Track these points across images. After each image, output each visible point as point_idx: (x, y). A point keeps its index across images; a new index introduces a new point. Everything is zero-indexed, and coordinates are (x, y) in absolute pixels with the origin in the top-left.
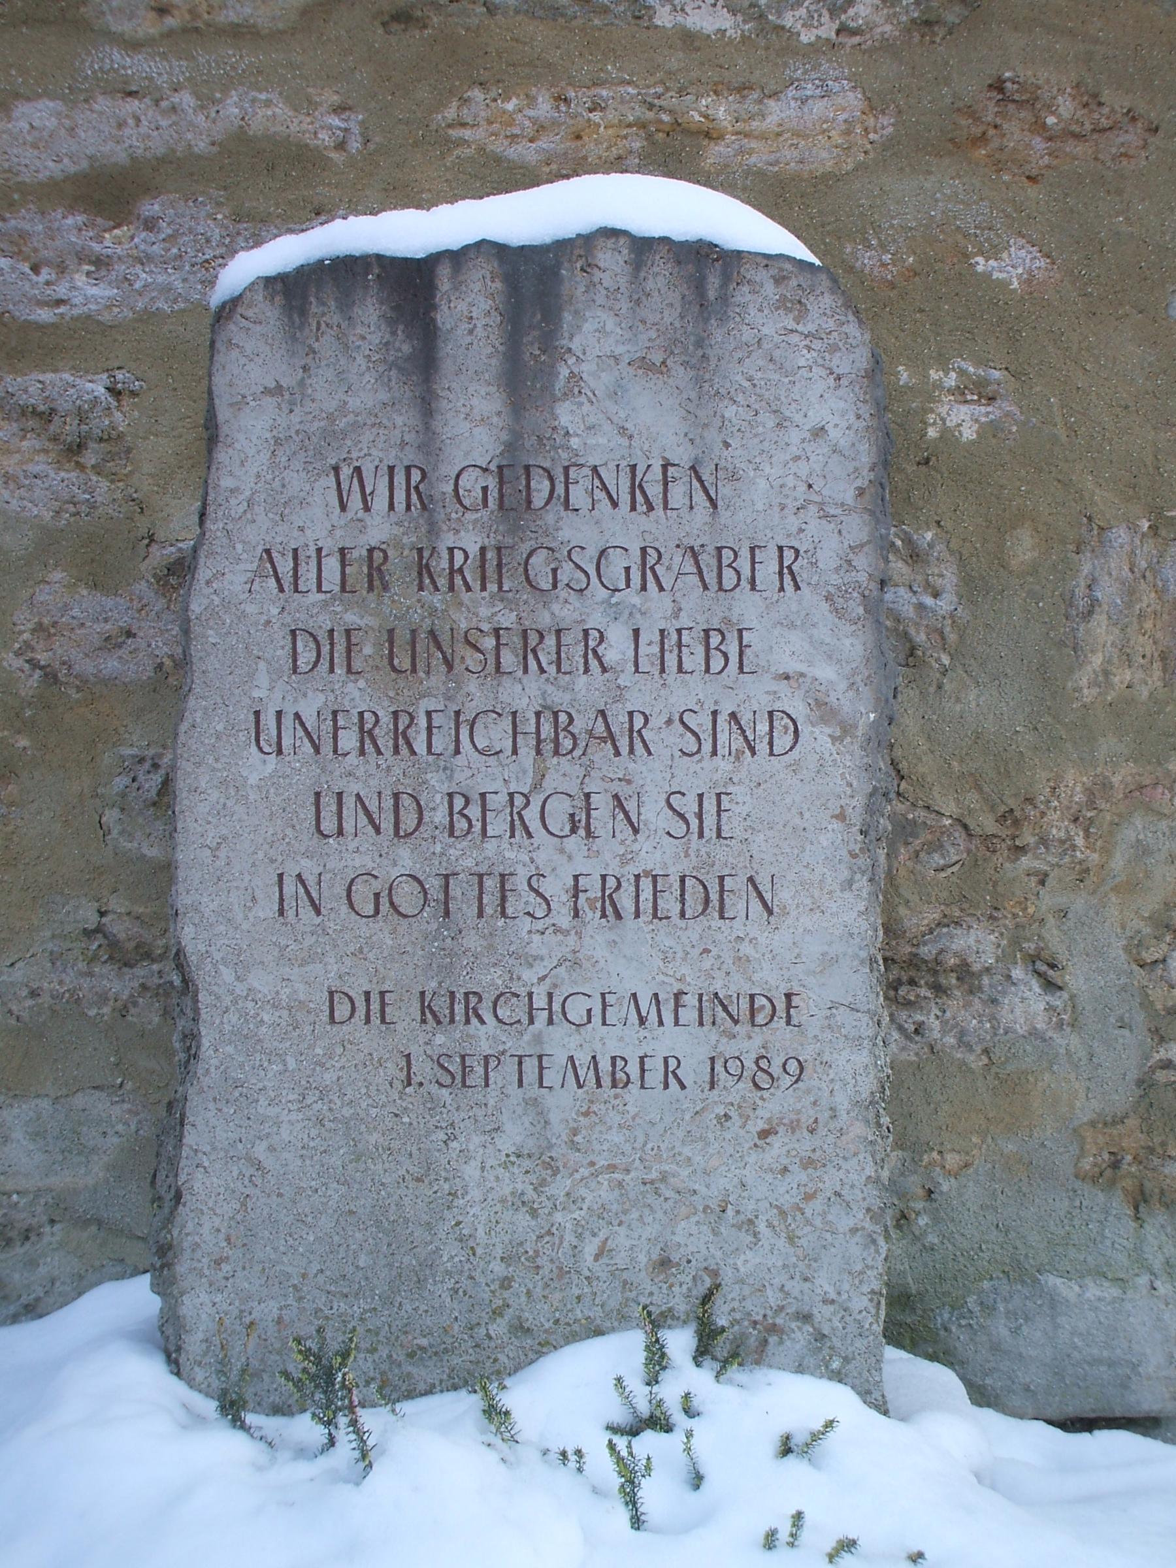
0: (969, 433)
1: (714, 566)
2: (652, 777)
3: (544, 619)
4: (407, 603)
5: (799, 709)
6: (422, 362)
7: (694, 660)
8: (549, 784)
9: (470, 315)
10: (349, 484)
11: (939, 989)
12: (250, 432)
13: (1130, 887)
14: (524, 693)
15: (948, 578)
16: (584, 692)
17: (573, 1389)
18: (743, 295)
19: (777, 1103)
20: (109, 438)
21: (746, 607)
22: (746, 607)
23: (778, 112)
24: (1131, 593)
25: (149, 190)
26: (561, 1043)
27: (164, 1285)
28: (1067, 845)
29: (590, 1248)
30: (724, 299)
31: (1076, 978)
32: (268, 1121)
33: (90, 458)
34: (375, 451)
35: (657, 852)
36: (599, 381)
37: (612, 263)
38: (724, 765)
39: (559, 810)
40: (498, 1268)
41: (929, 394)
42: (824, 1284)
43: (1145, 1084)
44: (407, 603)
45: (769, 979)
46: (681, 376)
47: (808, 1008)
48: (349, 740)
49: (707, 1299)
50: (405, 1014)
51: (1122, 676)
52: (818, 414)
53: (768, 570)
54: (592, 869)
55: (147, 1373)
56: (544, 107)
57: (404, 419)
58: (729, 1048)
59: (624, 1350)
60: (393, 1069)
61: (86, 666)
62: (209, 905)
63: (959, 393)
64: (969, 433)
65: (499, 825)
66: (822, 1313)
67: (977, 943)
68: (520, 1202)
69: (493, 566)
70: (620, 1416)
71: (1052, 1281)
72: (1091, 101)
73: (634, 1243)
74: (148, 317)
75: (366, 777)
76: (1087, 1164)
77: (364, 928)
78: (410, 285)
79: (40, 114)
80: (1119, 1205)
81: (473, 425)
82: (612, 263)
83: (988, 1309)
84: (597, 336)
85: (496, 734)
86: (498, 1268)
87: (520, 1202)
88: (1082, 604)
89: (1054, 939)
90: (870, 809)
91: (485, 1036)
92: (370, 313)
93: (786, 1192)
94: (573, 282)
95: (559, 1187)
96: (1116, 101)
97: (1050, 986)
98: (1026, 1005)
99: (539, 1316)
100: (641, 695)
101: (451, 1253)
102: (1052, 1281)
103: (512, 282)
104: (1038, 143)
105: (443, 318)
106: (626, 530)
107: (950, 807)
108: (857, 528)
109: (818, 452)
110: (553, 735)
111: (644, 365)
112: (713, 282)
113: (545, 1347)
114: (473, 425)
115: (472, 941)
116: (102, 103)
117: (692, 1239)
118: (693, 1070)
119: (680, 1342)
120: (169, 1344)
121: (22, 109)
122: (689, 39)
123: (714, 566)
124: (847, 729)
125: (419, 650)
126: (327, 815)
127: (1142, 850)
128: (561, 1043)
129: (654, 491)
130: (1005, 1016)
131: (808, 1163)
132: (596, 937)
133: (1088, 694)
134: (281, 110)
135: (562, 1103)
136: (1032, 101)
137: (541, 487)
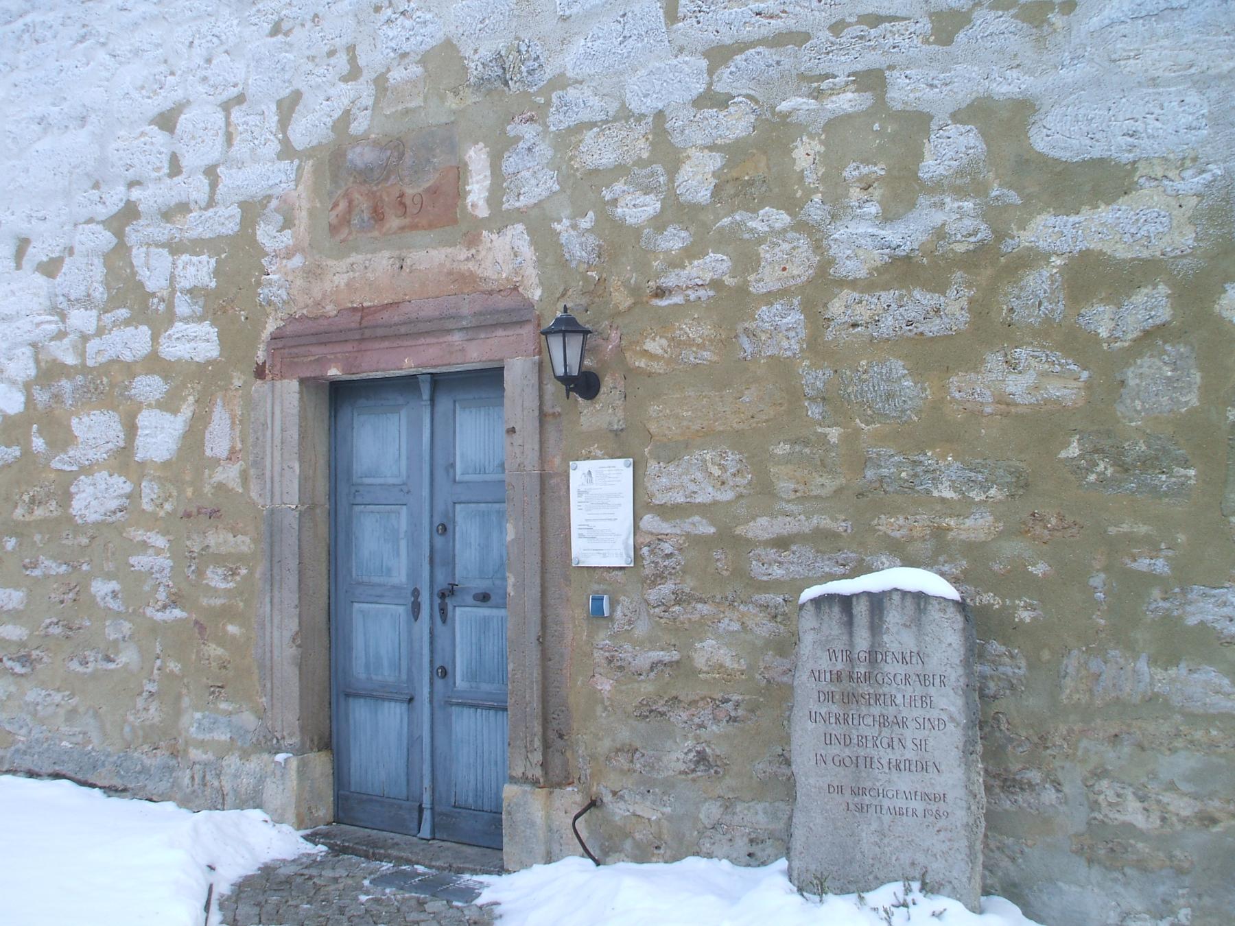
0: (1028, 620)
1: (923, 679)
2: (909, 734)
3: (881, 691)
4: (847, 686)
5: (945, 718)
6: (849, 623)
7: (919, 704)
8: (883, 734)
9: (861, 610)
10: (832, 654)
11: (1022, 789)
12: (808, 640)
13: (1083, 761)
14: (876, 710)
15: (1023, 663)
16: (891, 711)
17: (884, 895)
18: (930, 607)
19: (942, 823)
20: (784, 614)
21: (932, 691)
22: (932, 691)
23: (969, 522)
24: (1078, 671)
25: (794, 543)
26: (886, 803)
27: (788, 859)
28: (1061, 746)
29: (894, 858)
30: (925, 609)
31: (1066, 789)
32: (814, 817)
33: (779, 619)
34: (839, 645)
35: (910, 754)
36: (893, 629)
37: (896, 597)
38: (927, 732)
39: (885, 741)
40: (871, 861)
41: (1015, 608)
42: (955, 874)
43: (1089, 824)
44: (847, 686)
45: (939, 790)
46: (914, 628)
47: (949, 797)
48: (833, 720)
49: (924, 875)
50: (847, 792)
51: (1076, 697)
52: (949, 640)
53: (937, 681)
54: (893, 758)
55: (783, 881)
56: (901, 521)
57: (845, 638)
58: (929, 807)
59: (898, 887)
60: (844, 806)
61: (779, 679)
62: (799, 760)
63: (1025, 608)
64: (1028, 620)
65: (870, 744)
66: (955, 882)
67: (1034, 776)
68: (876, 844)
69: (868, 677)
70: (895, 902)
71: (1060, 884)
72: (1061, 518)
73: (905, 858)
74: (793, 579)
75: (837, 730)
76: (1074, 847)
77: (837, 769)
78: (846, 602)
79: (763, 521)
80: (1084, 863)
81: (862, 641)
82: (896, 597)
83: (1041, 891)
84: (893, 617)
85: (869, 721)
86: (871, 861)
87: (876, 844)
88: (1063, 674)
89: (1060, 776)
90: (965, 746)
91: (867, 799)
92: (836, 609)
93: (944, 847)
94: (887, 603)
95: (886, 841)
96: (1070, 519)
97: (1058, 791)
98: (1049, 796)
99: (881, 875)
100: (905, 712)
101: (859, 856)
102: (1060, 884)
103: (872, 604)
104: (1046, 532)
105: (854, 612)
106: (901, 669)
107: (1024, 734)
108: (960, 671)
109: (950, 650)
110: (883, 722)
111: (905, 625)
112: (922, 604)
113: (882, 883)
114: (862, 641)
115: (864, 774)
116: (780, 518)
117: (920, 858)
118: (920, 812)
119: (916, 885)
120: (789, 874)
121: (759, 519)
122: (943, 500)
123: (923, 679)
124: (958, 724)
125: (849, 698)
126: (828, 739)
127: (1087, 750)
128: (886, 803)
129: (908, 659)
130: (1042, 799)
131: (950, 840)
132: (895, 775)
133: (1065, 701)
134: (828, 521)
135: (887, 818)
136: (1043, 520)
137: (880, 657)
